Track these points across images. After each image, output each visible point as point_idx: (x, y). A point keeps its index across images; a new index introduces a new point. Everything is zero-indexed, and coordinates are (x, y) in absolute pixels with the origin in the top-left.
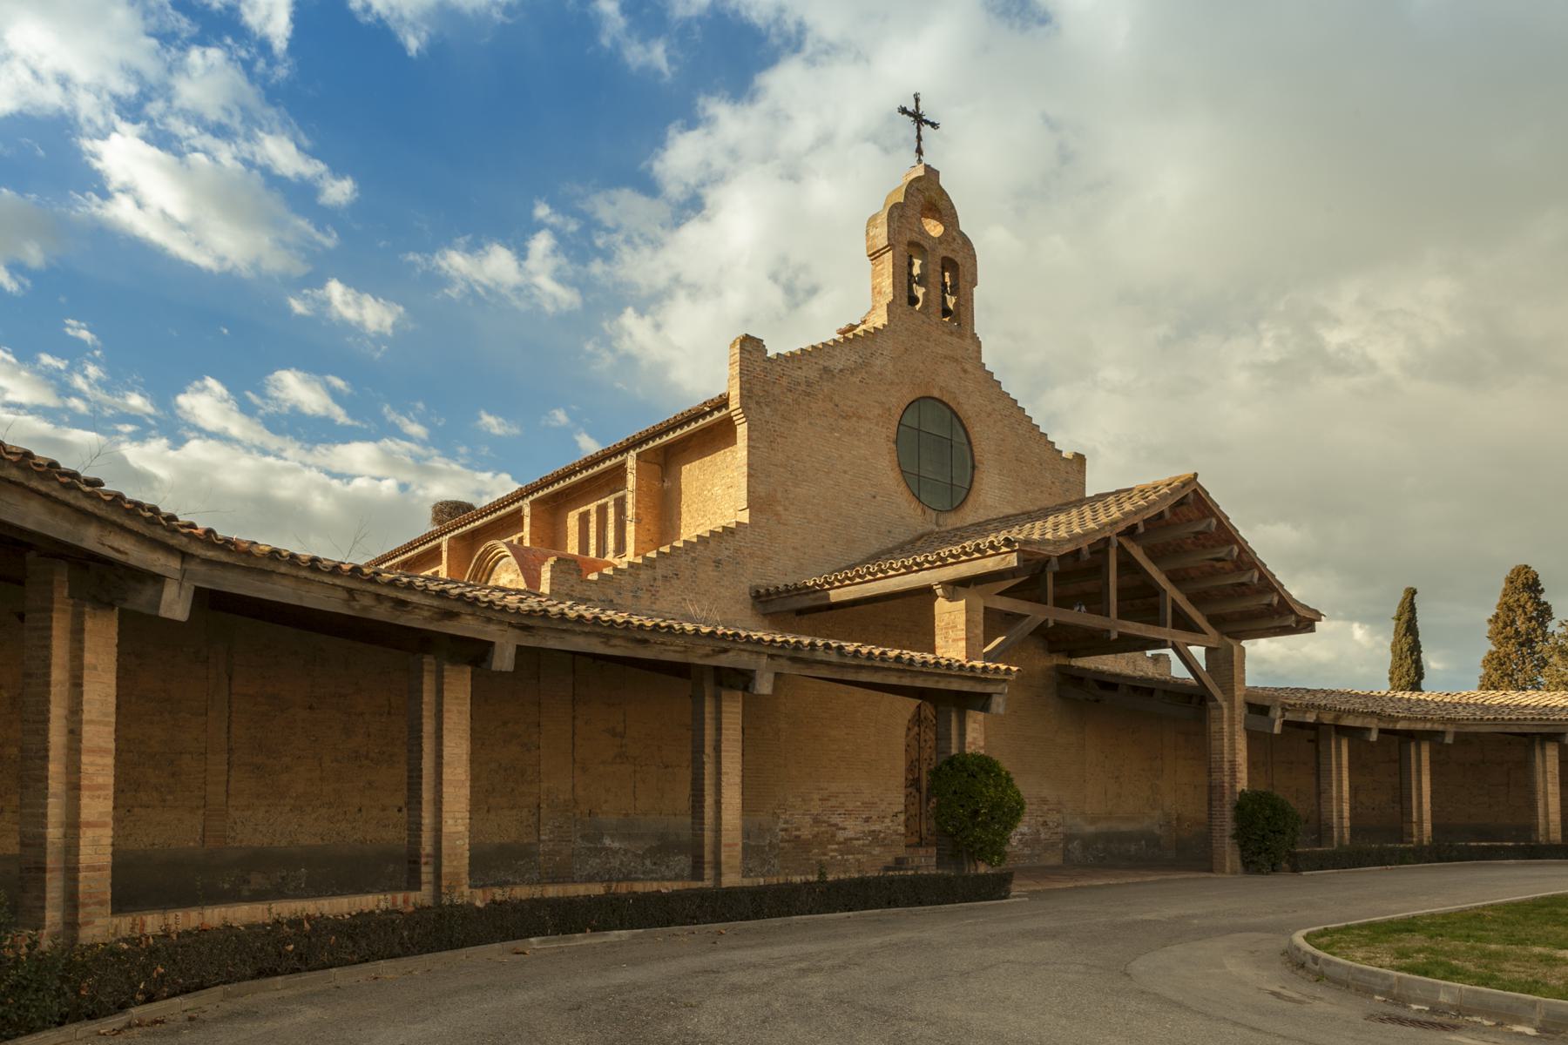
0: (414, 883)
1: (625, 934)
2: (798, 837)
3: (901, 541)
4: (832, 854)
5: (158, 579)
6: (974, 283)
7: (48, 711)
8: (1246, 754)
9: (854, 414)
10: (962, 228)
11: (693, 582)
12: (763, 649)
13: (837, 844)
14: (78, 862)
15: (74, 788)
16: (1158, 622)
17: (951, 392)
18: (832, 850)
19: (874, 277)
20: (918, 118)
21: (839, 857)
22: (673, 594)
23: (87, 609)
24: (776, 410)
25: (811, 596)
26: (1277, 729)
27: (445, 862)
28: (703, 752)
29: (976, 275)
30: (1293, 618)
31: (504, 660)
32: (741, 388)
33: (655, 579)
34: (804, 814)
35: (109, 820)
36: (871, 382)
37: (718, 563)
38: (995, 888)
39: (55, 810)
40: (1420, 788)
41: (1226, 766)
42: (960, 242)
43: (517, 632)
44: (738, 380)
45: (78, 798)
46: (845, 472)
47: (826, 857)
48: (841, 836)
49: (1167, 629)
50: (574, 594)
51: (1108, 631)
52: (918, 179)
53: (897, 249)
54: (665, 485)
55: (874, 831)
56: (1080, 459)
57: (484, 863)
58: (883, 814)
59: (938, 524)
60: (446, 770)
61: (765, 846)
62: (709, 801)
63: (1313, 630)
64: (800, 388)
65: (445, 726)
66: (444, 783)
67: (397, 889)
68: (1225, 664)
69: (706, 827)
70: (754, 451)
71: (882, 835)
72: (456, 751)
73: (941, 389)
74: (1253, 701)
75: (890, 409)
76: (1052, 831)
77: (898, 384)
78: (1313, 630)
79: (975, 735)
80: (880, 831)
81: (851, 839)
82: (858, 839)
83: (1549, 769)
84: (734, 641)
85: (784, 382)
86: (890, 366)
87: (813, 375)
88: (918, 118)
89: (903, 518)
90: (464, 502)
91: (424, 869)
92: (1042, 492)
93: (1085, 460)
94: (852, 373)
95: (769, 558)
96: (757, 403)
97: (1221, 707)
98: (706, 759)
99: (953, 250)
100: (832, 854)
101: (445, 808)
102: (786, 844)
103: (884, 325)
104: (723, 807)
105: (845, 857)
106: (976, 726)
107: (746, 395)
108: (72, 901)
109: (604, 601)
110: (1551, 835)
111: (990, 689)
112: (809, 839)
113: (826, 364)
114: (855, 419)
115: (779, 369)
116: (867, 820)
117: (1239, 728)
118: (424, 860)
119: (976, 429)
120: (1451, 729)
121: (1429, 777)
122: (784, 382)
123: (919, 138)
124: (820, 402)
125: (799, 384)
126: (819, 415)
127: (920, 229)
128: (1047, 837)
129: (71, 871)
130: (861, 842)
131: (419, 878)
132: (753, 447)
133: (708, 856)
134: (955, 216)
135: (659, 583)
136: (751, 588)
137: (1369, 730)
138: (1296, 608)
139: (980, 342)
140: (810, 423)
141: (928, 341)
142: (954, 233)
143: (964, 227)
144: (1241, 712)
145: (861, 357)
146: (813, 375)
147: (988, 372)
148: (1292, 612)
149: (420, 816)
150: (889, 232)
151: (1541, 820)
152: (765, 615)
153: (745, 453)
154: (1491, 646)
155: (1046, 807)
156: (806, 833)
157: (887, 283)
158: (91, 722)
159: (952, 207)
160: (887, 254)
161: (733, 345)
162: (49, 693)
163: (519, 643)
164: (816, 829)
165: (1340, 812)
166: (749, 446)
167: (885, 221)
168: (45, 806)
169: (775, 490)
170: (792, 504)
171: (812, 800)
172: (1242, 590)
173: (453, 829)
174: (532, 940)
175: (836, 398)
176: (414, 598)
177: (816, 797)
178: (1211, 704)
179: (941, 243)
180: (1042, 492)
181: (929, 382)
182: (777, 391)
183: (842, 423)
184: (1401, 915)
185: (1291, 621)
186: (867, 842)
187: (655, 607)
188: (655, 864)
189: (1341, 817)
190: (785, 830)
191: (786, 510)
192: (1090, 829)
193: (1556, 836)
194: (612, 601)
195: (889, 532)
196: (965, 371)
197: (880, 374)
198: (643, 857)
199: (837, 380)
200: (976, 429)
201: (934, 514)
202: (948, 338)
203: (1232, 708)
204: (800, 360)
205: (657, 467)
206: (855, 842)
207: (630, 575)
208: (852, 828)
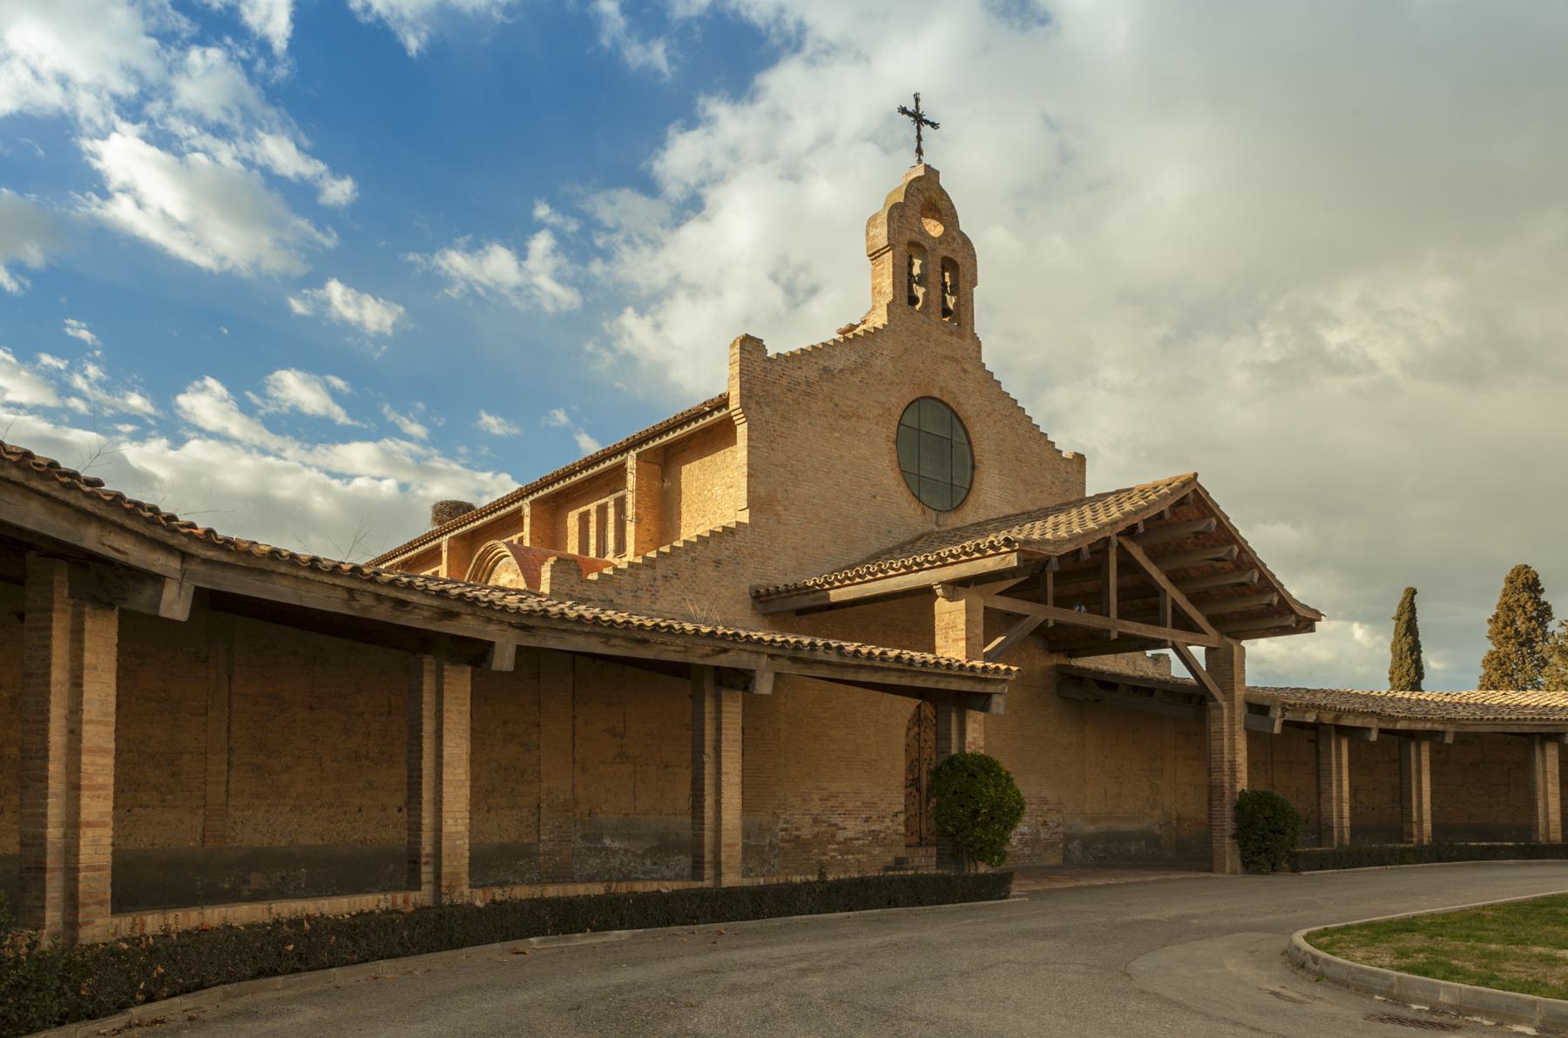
0: (414, 883)
1: (624, 934)
2: (797, 837)
3: (901, 541)
4: (832, 854)
5: (158, 579)
6: (974, 283)
7: (48, 711)
8: (1246, 754)
10: (962, 228)
11: (694, 582)
12: (763, 649)
13: (837, 843)
14: (78, 862)
16: (1158, 622)
17: (951, 392)
18: (832, 850)
20: (918, 118)
21: (839, 857)
22: (673, 594)
24: (776, 410)
25: (812, 596)
26: (1277, 729)
27: (445, 862)
28: (703, 752)
31: (504, 660)
32: (741, 388)
33: (655, 579)
35: (109, 820)
36: (871, 382)
37: (718, 563)
38: (995, 888)
39: (55, 810)
40: (1420, 788)
41: (1226, 766)
42: (960, 242)
44: (738, 379)
45: (78, 798)
46: (845, 472)
48: (841, 836)
49: (1167, 629)
50: (574, 594)
51: (1108, 631)
52: (918, 179)
53: (898, 249)
54: (665, 485)
56: (1080, 459)
57: (484, 863)
58: (882, 814)
59: (937, 525)
60: (446, 770)
61: (765, 846)
62: (709, 801)
63: (1313, 630)
65: (445, 726)
67: (397, 889)
68: (1225, 664)
69: (706, 827)
71: (882, 835)
73: (941, 389)
75: (890, 409)
76: (1051, 831)
77: (897, 384)
78: (1313, 630)
79: (975, 735)
80: (880, 831)
81: (851, 839)
82: (858, 839)
85: (784, 381)
86: (890, 366)
87: (813, 375)
88: (918, 118)
89: (902, 518)
91: (424, 869)
94: (852, 373)
95: (769, 558)
96: (757, 403)
97: (1221, 707)
98: (706, 759)
100: (832, 854)
101: (445, 808)
102: (786, 844)
103: (884, 325)
104: (723, 807)
108: (72, 901)
110: (1551, 835)
111: (990, 689)
113: (825, 364)
114: (855, 419)
115: (779, 369)
116: (867, 820)
117: (1239, 727)
118: (424, 860)
119: (976, 429)
120: (1451, 729)
122: (784, 381)
123: (919, 138)
124: (820, 402)
125: (799, 384)
126: (820, 415)
128: (1047, 837)
129: (71, 871)
130: (861, 842)
135: (659, 583)
137: (1369, 729)
138: (1296, 608)
139: (980, 342)
140: (810, 423)
142: (954, 233)
143: (964, 227)
144: (1241, 712)
145: (860, 357)
146: (813, 375)
148: (1292, 612)
149: (420, 816)
150: (889, 232)
151: (1541, 820)
153: (745, 453)
154: (1490, 646)
156: (806, 833)
158: (91, 722)
159: (952, 207)
162: (49, 692)
164: (816, 829)
165: (1340, 812)
166: (749, 446)
167: (885, 221)
168: (45, 806)
169: (775, 490)
171: (812, 800)
172: (1242, 590)
173: (453, 829)
174: (532, 939)
175: (836, 399)
178: (1211, 704)
179: (941, 243)
182: (777, 391)
183: (843, 423)
185: (1291, 621)
186: (867, 842)
187: (654, 607)
189: (1341, 817)
190: (786, 830)
191: (786, 510)
192: (1090, 829)
193: (1556, 836)
194: (612, 601)
195: (889, 532)
196: (965, 371)
197: (880, 374)
198: (643, 857)
199: (837, 380)
200: (976, 429)
201: (934, 514)
202: (948, 338)
203: (1232, 707)
206: (855, 842)
208: (852, 828)
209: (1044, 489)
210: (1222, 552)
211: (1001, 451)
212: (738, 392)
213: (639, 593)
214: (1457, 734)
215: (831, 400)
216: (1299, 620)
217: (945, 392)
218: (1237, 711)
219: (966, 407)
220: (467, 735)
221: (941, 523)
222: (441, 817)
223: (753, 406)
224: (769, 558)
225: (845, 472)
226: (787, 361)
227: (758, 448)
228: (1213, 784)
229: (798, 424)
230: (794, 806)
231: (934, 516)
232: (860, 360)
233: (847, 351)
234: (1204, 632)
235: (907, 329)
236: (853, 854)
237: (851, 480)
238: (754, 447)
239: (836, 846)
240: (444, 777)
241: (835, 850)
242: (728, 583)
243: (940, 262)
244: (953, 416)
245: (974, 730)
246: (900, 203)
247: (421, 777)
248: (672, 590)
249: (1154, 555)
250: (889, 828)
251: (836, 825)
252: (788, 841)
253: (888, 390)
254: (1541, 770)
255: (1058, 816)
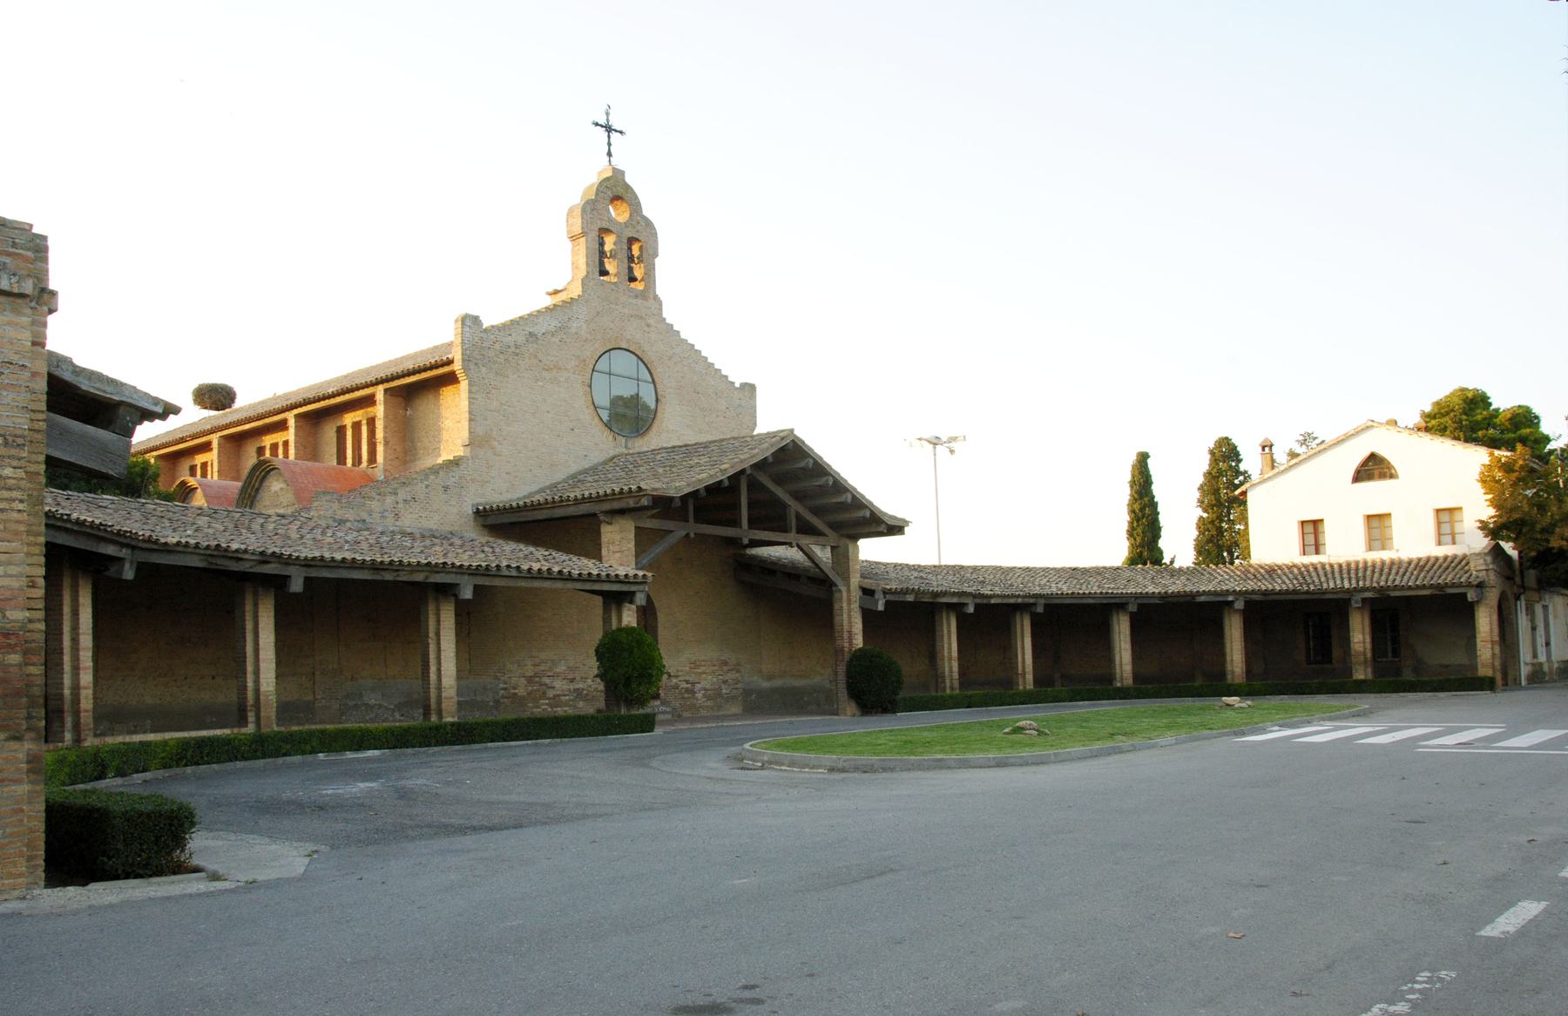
0: (243, 721)
1: (376, 753)
2: (515, 694)
3: (595, 462)
4: (543, 707)
5: (121, 560)
6: (656, 255)
7: (62, 629)
8: (861, 626)
9: (555, 366)
10: (645, 213)
11: (427, 503)
12: (464, 571)
13: (549, 699)
14: (79, 707)
15: (76, 669)
16: (785, 530)
17: (636, 343)
18: (543, 704)
19: (573, 256)
20: (609, 129)
21: (550, 710)
22: (411, 513)
23: (80, 575)
24: (491, 368)
25: (517, 514)
26: (881, 607)
27: (262, 710)
28: (428, 636)
29: (657, 249)
30: (883, 526)
31: (297, 586)
32: (463, 354)
33: (397, 503)
34: (519, 677)
35: (91, 685)
36: (568, 341)
37: (446, 488)
38: (647, 724)
39: (67, 681)
40: (1023, 648)
41: (846, 635)
42: (643, 224)
43: (304, 569)
44: (460, 347)
45: (78, 674)
46: (548, 412)
47: (539, 710)
48: (551, 693)
49: (792, 534)
50: (336, 517)
51: (741, 539)
52: (607, 179)
53: (590, 235)
54: (408, 413)
55: (578, 689)
56: (749, 389)
57: (286, 710)
58: (585, 676)
59: (626, 447)
60: (261, 652)
61: (489, 702)
62: (433, 669)
63: (903, 533)
64: (510, 350)
65: (260, 626)
66: (261, 661)
67: (234, 727)
68: (843, 558)
69: (431, 686)
70: (474, 401)
71: (585, 692)
72: (267, 641)
73: (628, 341)
74: (864, 586)
75: (584, 361)
76: (732, 687)
77: (591, 341)
78: (903, 533)
79: (629, 619)
80: (583, 689)
81: (559, 696)
82: (565, 695)
83: (1122, 630)
84: (444, 567)
85: (497, 346)
86: (584, 326)
87: (521, 340)
88: (609, 129)
89: (597, 444)
90: (216, 384)
91: (249, 714)
92: (717, 416)
93: (755, 388)
94: (553, 335)
95: (486, 482)
96: (476, 364)
97: (840, 591)
98: (430, 641)
99: (637, 231)
100: (543, 707)
101: (261, 676)
102: (506, 700)
103: (579, 296)
104: (443, 673)
105: (555, 709)
106: (631, 613)
107: (466, 360)
108: (77, 726)
109: (358, 521)
110: (1124, 681)
111: (633, 588)
112: (524, 696)
113: (531, 330)
114: (555, 370)
115: (492, 337)
116: (572, 680)
117: (855, 606)
118: (249, 708)
119: (659, 370)
120: (1042, 601)
121: (1030, 639)
122: (497, 346)
123: (609, 144)
124: (527, 360)
125: (509, 347)
126: (526, 369)
127: (609, 218)
128: (728, 692)
129: (76, 713)
130: (567, 698)
131: (247, 720)
132: (474, 398)
133: (433, 705)
134: (639, 204)
135: (401, 505)
136: (473, 505)
137: (966, 604)
138: (885, 519)
139: (661, 302)
140: (519, 377)
141: (617, 304)
142: (639, 218)
143: (646, 212)
144: (856, 594)
145: (560, 322)
146: (521, 340)
147: (668, 324)
148: (883, 522)
149: (246, 682)
150: (582, 223)
151: (1118, 671)
152: (484, 526)
153: (467, 403)
154: (1199, 512)
155: (725, 668)
156: (521, 692)
157: (582, 261)
158: (83, 634)
159: (636, 197)
160: (581, 239)
161: (456, 321)
162: (62, 619)
163: (307, 575)
164: (530, 688)
165: (951, 668)
166: (469, 398)
167: (580, 213)
168: (62, 678)
169: (491, 430)
170: (505, 439)
171: (526, 665)
172: (844, 507)
173: (267, 689)
174: (320, 754)
175: (540, 355)
176: (246, 556)
177: (529, 663)
178: (834, 588)
179: (626, 227)
180: (717, 416)
181: (617, 337)
182: (491, 354)
183: (545, 374)
184: (782, 720)
185: (882, 528)
186: (572, 698)
187: (397, 523)
188: (402, 715)
189: (951, 671)
190: (505, 689)
191: (500, 444)
192: (766, 685)
193: (1129, 681)
194: (365, 520)
195: (586, 456)
196: (648, 326)
197: (576, 334)
198: (393, 710)
199: (540, 342)
200: (659, 370)
201: (623, 440)
202: (634, 301)
203: (849, 591)
204: (509, 329)
205: (401, 399)
206: (562, 698)
207: (378, 500)
208: (560, 685)
209: (719, 413)
210: (822, 481)
211: (681, 386)
212: (460, 357)
213: (386, 514)
214: (1046, 605)
215: (536, 356)
216: (894, 528)
217: (631, 343)
218: (853, 594)
219: (649, 353)
220: (273, 631)
221: (629, 446)
222: (259, 681)
223: (472, 367)
224: (486, 482)
225: (548, 412)
226: (499, 331)
227: (477, 399)
228: (26, 715)
229: (508, 377)
230: (511, 671)
231: (624, 441)
232: (560, 325)
233: (548, 318)
234: (825, 535)
235: (598, 297)
236: (561, 707)
237: (552, 418)
238: (474, 398)
239: (547, 701)
240: (260, 656)
241: (547, 704)
242: (455, 503)
243: (626, 241)
244: (640, 362)
245: (628, 616)
246: (592, 200)
247: (246, 657)
248: (411, 511)
249: (779, 481)
250: (590, 687)
251: (546, 685)
252: (506, 698)
253: (583, 346)
254: (1117, 631)
255: (737, 675)
